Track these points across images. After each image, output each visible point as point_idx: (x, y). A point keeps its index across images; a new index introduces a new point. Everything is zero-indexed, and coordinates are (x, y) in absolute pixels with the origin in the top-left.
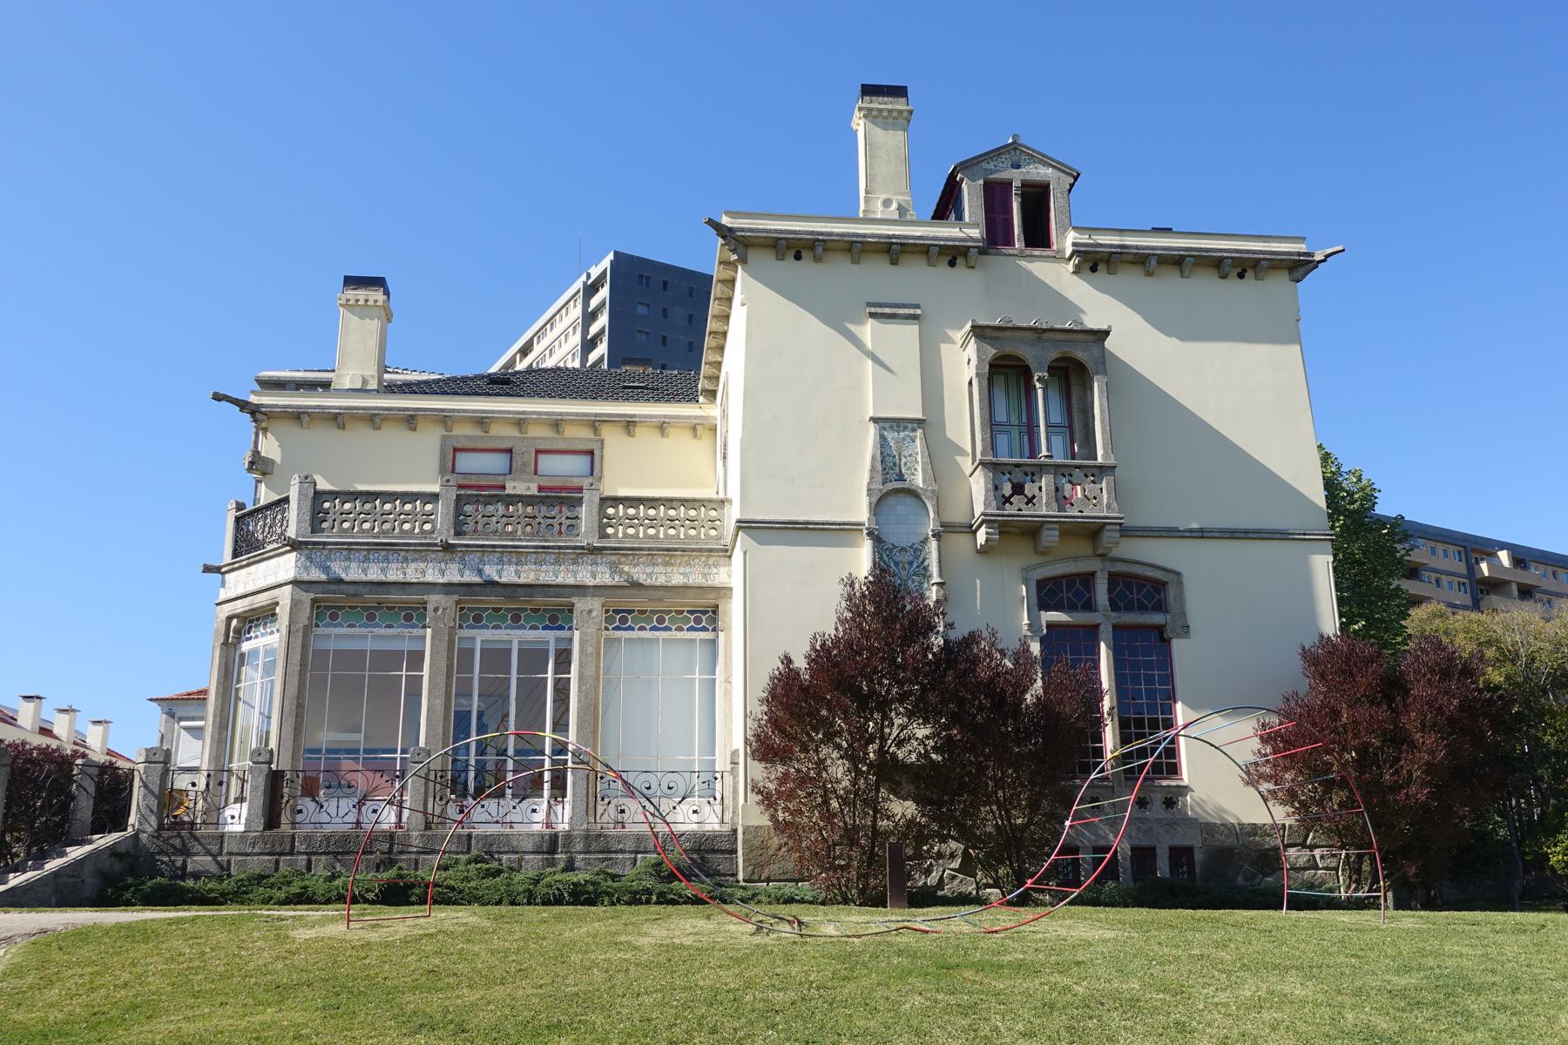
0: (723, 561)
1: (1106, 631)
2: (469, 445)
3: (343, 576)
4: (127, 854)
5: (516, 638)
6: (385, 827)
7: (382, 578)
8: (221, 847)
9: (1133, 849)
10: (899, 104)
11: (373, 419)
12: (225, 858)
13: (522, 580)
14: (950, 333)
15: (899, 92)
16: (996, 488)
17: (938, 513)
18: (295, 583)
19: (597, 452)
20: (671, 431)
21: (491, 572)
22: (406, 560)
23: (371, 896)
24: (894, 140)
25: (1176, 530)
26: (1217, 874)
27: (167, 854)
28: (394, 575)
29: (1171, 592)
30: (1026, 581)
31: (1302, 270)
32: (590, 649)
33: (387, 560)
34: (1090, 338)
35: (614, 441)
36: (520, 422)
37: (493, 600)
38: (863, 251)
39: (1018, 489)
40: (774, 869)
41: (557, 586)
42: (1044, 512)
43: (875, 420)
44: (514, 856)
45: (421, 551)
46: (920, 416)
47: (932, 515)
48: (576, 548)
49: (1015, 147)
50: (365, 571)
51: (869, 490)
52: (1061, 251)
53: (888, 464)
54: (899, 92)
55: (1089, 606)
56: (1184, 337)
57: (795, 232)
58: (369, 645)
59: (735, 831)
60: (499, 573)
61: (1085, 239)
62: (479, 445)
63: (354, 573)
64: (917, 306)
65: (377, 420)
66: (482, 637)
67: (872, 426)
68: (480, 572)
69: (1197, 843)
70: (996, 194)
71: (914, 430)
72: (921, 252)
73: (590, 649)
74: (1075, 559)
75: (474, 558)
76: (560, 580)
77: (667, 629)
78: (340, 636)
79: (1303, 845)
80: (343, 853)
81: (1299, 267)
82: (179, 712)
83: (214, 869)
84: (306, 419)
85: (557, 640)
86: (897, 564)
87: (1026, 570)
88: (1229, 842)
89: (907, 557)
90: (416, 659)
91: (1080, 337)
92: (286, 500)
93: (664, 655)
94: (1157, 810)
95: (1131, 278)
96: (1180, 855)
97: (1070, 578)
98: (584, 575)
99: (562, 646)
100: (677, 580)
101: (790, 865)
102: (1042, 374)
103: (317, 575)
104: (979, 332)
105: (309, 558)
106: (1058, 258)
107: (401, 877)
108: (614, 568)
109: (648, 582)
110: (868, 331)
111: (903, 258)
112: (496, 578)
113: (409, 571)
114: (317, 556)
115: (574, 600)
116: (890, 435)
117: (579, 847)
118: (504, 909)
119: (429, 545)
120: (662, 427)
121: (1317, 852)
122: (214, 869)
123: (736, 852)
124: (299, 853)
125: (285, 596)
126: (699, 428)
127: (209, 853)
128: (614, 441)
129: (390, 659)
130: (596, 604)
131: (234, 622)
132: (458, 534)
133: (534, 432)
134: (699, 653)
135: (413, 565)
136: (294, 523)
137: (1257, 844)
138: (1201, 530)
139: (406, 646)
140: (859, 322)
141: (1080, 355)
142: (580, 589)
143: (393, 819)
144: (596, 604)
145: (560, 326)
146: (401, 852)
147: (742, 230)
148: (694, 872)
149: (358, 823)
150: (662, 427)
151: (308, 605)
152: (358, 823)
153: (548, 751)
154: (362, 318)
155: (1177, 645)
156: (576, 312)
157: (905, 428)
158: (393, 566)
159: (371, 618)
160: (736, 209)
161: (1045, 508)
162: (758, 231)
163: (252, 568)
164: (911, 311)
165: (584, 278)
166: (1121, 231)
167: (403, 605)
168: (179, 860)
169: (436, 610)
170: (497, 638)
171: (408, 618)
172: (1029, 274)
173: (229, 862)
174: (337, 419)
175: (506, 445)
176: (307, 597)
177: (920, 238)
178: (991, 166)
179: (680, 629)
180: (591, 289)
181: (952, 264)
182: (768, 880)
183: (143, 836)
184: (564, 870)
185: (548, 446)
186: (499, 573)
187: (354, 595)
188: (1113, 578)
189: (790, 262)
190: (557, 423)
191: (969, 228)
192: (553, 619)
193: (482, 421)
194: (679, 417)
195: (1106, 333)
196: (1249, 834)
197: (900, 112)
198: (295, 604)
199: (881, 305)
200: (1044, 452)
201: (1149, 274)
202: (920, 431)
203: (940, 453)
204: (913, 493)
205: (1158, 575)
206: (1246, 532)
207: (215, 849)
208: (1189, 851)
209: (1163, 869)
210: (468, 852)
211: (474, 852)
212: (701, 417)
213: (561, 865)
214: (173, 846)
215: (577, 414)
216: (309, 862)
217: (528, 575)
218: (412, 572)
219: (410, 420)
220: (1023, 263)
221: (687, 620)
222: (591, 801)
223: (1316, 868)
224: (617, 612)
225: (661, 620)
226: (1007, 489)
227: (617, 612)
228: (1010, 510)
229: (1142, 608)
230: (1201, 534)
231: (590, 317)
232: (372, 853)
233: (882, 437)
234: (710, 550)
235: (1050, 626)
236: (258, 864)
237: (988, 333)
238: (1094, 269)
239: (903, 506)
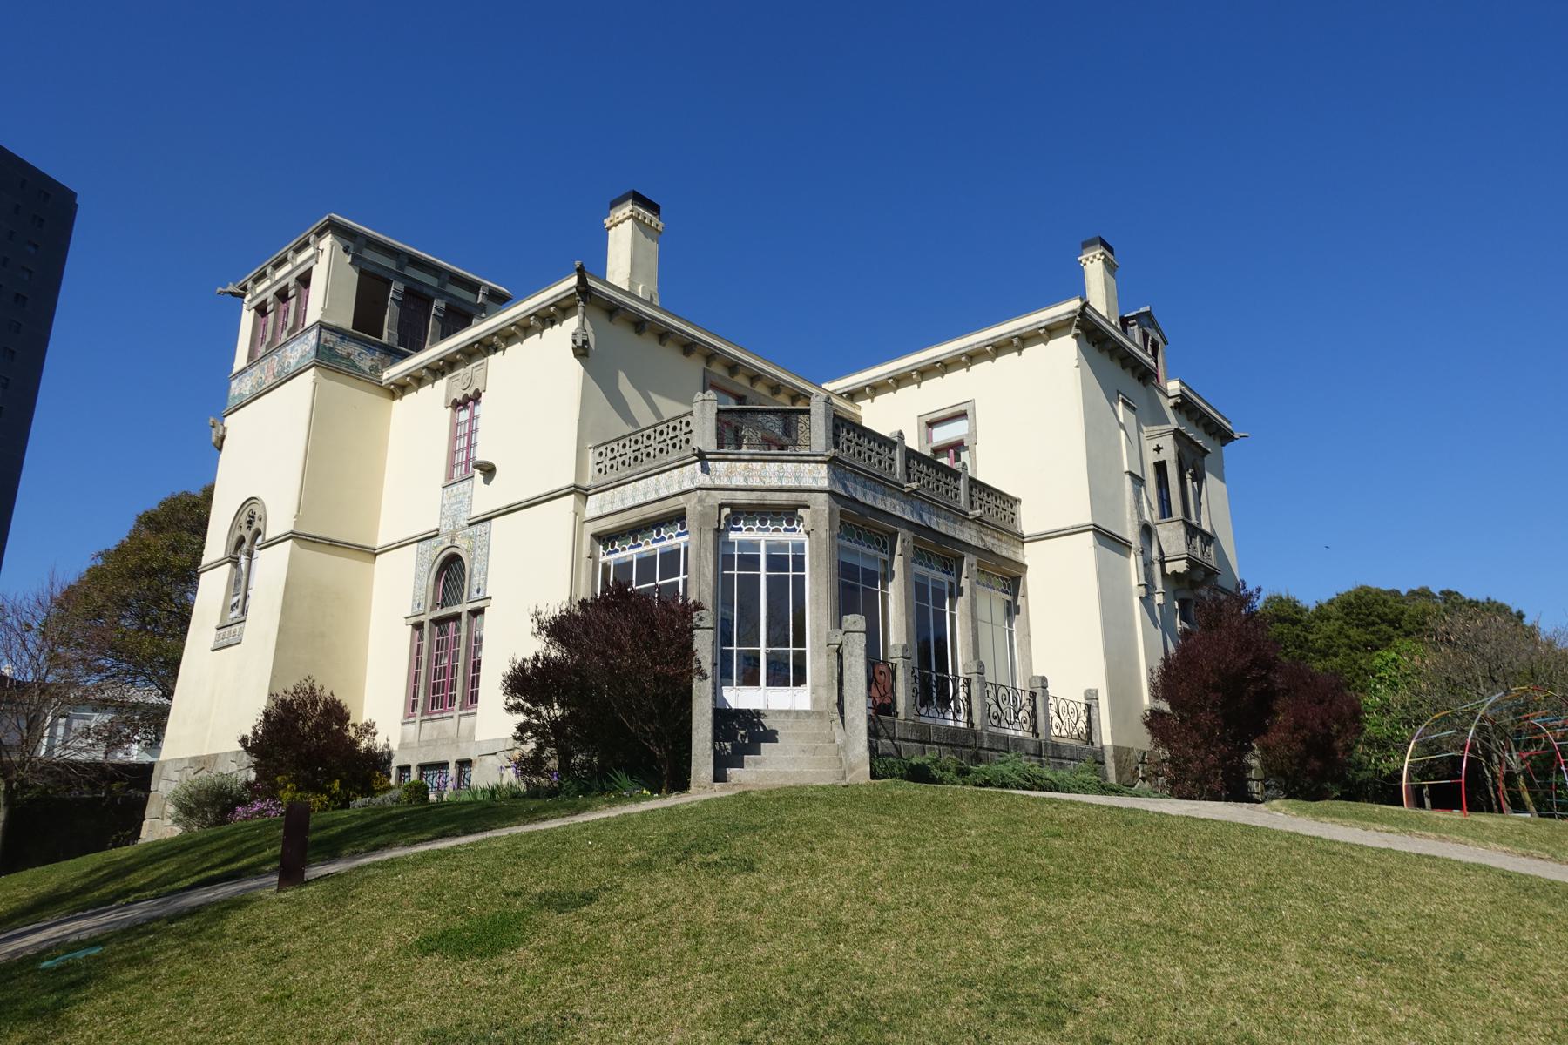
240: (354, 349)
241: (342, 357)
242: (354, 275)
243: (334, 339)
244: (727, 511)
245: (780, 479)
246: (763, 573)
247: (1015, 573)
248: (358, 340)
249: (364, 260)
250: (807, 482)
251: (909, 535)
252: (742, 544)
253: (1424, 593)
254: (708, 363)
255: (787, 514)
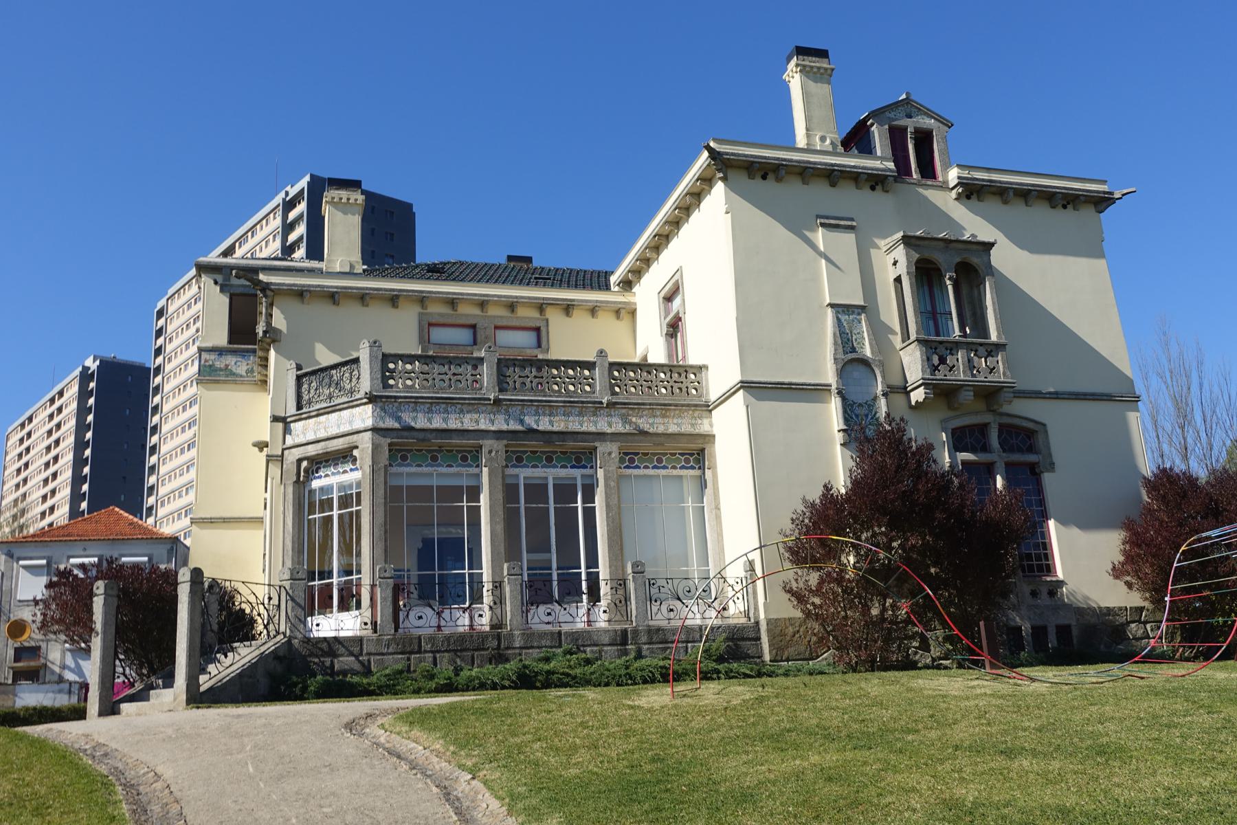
0: (705, 414)
1: (1000, 466)
2: (442, 321)
3: (413, 424)
4: (285, 657)
5: (552, 475)
6: (461, 629)
7: (444, 426)
8: (361, 649)
9: (1032, 628)
10: (823, 64)
11: (363, 297)
12: (365, 658)
13: (555, 429)
14: (876, 240)
15: (823, 54)
16: (928, 359)
17: (883, 377)
18: (374, 430)
19: (543, 329)
20: (600, 313)
21: (530, 421)
22: (462, 411)
23: (507, 683)
24: (823, 90)
25: (1040, 393)
26: (1090, 640)
27: (317, 656)
28: (453, 424)
29: (1041, 438)
30: (944, 430)
31: (1104, 205)
32: (612, 484)
33: (446, 411)
34: (980, 248)
35: (556, 319)
36: (483, 303)
37: (533, 444)
38: (813, 175)
39: (942, 360)
40: (791, 651)
41: (583, 433)
42: (962, 377)
43: (832, 305)
44: (595, 648)
45: (477, 404)
46: (862, 303)
47: (879, 379)
48: (595, 403)
49: (907, 101)
50: (430, 420)
51: (835, 359)
52: (946, 182)
53: (845, 341)
54: (823, 54)
55: (985, 448)
56: (1022, 246)
57: (765, 158)
58: (435, 482)
59: (757, 623)
60: (537, 422)
61: (965, 174)
62: (450, 321)
63: (421, 422)
64: (852, 220)
65: (367, 298)
66: (524, 474)
67: (829, 310)
68: (522, 422)
69: (1074, 623)
70: (897, 137)
71: (859, 314)
72: (851, 178)
73: (612, 484)
74: (977, 413)
75: (515, 410)
76: (584, 429)
77: (665, 467)
78: (413, 474)
79: (1139, 621)
80: (461, 651)
81: (1102, 202)
82: (17, 553)
83: (357, 667)
84: (307, 296)
85: (583, 476)
86: (857, 416)
87: (944, 421)
88: (1093, 620)
89: (863, 411)
90: (474, 493)
91: (975, 247)
92: (356, 361)
93: (663, 485)
94: (1044, 599)
95: (993, 205)
96: (1064, 631)
97: (971, 428)
98: (602, 424)
99: (588, 482)
100: (673, 429)
101: (802, 648)
102: (949, 274)
103: (391, 423)
104: (908, 241)
105: (383, 409)
106: (944, 187)
107: (525, 667)
108: (625, 420)
109: (651, 431)
110: (820, 237)
111: (842, 183)
112: (535, 427)
113: (466, 421)
114: (389, 407)
115: (597, 444)
116: (844, 318)
117: (644, 639)
118: (613, 689)
119: (480, 399)
120: (593, 310)
121: (1148, 626)
122: (357, 667)
123: (759, 639)
124: (426, 652)
125: (366, 441)
126: (623, 312)
127: (351, 654)
128: (556, 319)
129: (453, 493)
130: (613, 448)
131: (305, 464)
132: (501, 390)
133: (493, 311)
134: (689, 487)
135: (468, 416)
136: (366, 382)
137: (1111, 621)
138: (1056, 393)
139: (465, 482)
140: (814, 230)
141: (975, 260)
142: (601, 436)
143: (467, 622)
144: (613, 448)
145: (260, 235)
146: (508, 648)
147: (727, 154)
148: (733, 652)
149: (439, 627)
150: (593, 310)
151: (386, 448)
152: (439, 627)
153: (554, 565)
154: (345, 213)
155: (1047, 478)
156: (276, 222)
157: (853, 313)
158: (452, 416)
159: (434, 459)
160: (721, 137)
161: (961, 374)
162: (739, 155)
163: (322, 418)
164: (849, 223)
165: (282, 194)
166: (988, 170)
167: (465, 449)
168: (328, 661)
169: (490, 452)
170: (536, 475)
171: (464, 459)
172: (926, 198)
173: (369, 661)
174: (333, 297)
175: (472, 322)
176: (385, 442)
177: (854, 167)
178: (892, 115)
179: (674, 467)
180: (289, 205)
181: (873, 188)
182: (788, 660)
183: (295, 642)
184: (635, 659)
185: (505, 323)
186: (537, 422)
187: (423, 440)
188: (1002, 428)
189: (758, 182)
190: (512, 305)
191: (880, 161)
192: (578, 460)
193: (452, 302)
194: (608, 302)
195: (992, 245)
196: (1106, 615)
197: (826, 69)
198: (376, 448)
199: (827, 218)
200: (957, 332)
201: (1005, 202)
202: (863, 316)
203: (879, 332)
204: (864, 362)
205: (1031, 425)
206: (1085, 394)
207: (356, 650)
208: (1068, 627)
209: (1052, 642)
210: (560, 646)
211: (565, 646)
212: (625, 303)
213: (632, 655)
214: (321, 649)
215: (529, 298)
216: (435, 659)
217: (559, 424)
218: (468, 422)
219: (394, 299)
220: (920, 190)
221: (679, 461)
222: (620, 604)
223: (1148, 637)
224: (626, 454)
225: (660, 461)
226: (936, 360)
227: (626, 454)
228: (939, 376)
229: (1020, 450)
230: (1056, 396)
231: (288, 228)
232: (484, 649)
233: (839, 320)
234: (696, 406)
235: (963, 463)
236: (395, 662)
237: (913, 241)
238: (968, 197)
239: (858, 372)
240: (230, 360)
241: (221, 370)
242: (225, 300)
243: (213, 357)
244: (305, 464)
245: (339, 426)
246: (354, 509)
247: (514, 482)
248: (234, 352)
249: (232, 286)
250: (358, 425)
251: (498, 445)
252: (321, 489)
253: (141, 696)
254: (423, 307)
255: (344, 456)
